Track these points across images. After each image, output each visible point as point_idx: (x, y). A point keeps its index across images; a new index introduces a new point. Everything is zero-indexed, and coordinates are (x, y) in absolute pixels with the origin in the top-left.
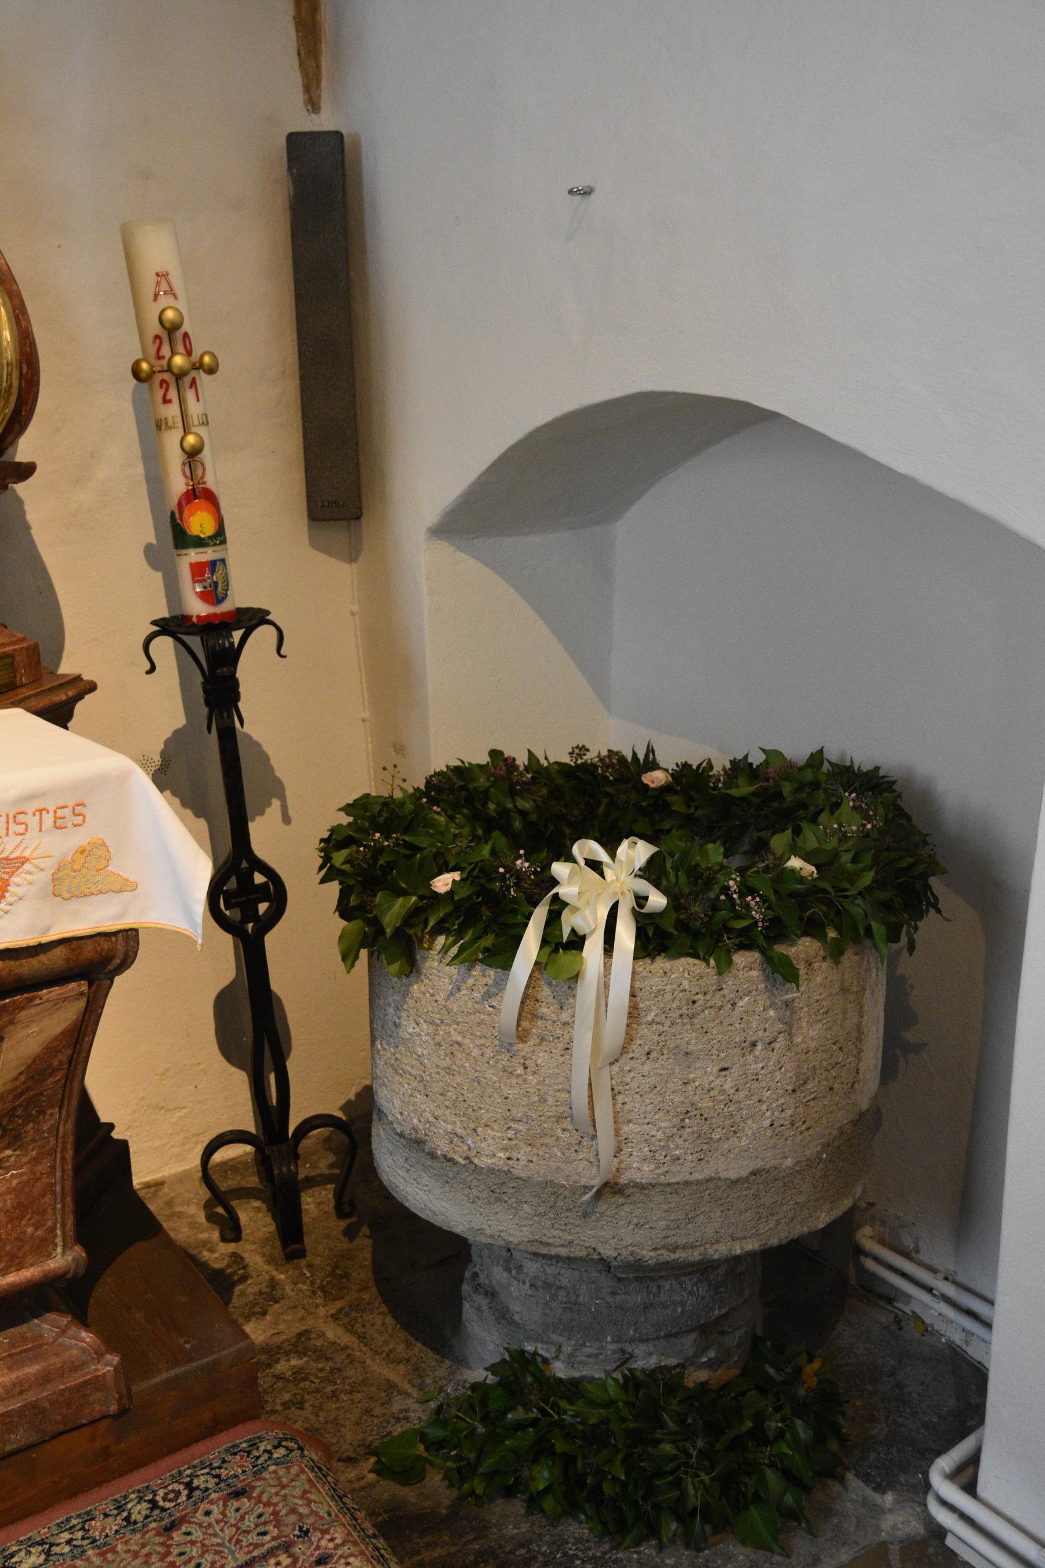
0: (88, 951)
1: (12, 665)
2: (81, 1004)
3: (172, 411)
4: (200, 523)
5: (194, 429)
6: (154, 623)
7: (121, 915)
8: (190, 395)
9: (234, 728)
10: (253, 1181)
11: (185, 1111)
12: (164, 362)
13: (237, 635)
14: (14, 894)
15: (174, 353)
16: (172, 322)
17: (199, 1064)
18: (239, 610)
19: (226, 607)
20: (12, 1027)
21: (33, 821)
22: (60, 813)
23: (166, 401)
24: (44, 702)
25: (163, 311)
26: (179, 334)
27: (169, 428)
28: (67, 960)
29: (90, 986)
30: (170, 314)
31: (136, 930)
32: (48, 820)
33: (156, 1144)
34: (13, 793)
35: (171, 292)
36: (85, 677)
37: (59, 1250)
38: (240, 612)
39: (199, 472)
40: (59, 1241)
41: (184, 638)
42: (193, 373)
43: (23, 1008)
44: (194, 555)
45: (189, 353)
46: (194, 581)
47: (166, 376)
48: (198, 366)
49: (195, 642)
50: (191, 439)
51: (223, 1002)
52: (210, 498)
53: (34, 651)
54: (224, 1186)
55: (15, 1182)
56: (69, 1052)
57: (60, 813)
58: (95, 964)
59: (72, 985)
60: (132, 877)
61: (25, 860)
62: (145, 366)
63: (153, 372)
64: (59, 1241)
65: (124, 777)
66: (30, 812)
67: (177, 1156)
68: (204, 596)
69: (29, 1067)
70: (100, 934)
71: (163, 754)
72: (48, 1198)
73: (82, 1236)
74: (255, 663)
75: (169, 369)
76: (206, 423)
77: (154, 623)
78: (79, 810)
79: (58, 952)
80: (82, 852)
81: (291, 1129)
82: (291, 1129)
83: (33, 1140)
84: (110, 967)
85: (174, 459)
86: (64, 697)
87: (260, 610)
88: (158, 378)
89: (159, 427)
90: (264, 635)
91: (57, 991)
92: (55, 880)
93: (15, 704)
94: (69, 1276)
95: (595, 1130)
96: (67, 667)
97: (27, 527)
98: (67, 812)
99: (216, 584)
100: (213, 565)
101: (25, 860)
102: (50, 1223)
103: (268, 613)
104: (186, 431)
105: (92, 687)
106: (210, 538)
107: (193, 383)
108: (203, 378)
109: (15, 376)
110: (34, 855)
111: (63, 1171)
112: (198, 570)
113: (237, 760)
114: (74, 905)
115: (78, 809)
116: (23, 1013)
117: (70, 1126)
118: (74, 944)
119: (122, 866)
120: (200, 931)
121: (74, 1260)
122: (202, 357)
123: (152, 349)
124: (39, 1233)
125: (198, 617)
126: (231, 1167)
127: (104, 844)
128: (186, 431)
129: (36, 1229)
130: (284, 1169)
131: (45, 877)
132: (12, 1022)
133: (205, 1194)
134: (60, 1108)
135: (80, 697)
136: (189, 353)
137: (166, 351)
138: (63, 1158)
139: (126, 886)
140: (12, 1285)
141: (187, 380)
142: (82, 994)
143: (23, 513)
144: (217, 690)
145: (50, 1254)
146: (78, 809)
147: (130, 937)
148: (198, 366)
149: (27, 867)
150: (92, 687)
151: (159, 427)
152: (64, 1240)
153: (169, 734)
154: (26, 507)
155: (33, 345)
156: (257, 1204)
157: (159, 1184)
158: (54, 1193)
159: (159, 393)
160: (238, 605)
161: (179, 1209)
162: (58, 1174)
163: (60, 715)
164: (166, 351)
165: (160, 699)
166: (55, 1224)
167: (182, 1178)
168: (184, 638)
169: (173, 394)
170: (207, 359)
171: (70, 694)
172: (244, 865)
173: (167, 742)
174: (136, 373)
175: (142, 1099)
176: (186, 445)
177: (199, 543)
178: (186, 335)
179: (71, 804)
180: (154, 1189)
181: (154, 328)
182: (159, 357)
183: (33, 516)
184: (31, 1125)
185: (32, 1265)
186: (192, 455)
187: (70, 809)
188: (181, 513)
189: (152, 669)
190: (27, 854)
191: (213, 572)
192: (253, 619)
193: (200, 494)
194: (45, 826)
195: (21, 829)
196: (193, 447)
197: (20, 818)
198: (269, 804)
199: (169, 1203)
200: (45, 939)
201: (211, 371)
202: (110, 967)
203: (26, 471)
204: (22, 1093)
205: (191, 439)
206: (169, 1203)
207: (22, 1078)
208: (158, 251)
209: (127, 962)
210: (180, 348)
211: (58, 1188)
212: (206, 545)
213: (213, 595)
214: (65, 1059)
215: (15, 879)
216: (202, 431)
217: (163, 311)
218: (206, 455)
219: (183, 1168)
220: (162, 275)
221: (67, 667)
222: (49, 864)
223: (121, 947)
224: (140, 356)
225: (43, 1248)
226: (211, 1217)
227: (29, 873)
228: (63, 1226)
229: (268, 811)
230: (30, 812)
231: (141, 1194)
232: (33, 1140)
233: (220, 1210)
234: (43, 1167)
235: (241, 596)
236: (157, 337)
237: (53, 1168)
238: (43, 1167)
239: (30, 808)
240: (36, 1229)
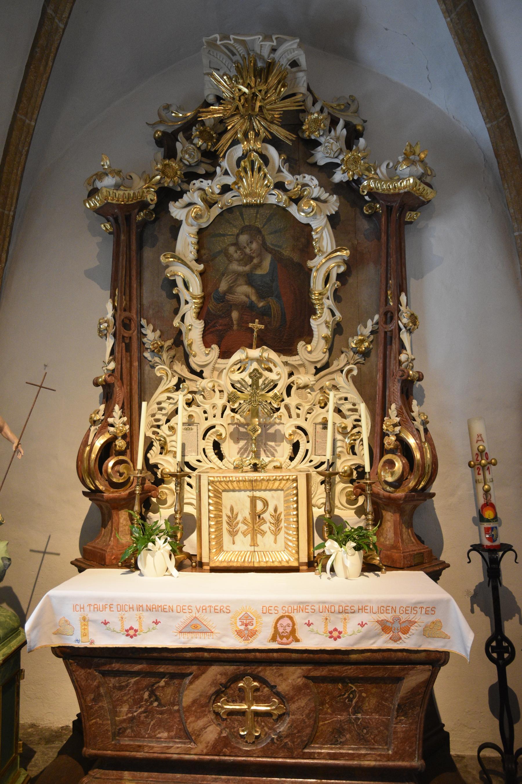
0: (433, 656)
1: (423, 556)
2: (429, 673)
3: (481, 477)
4: (489, 514)
5: (488, 484)
6: (471, 546)
7: (444, 646)
8: (487, 473)
9: (498, 587)
10: (500, 769)
11: (475, 730)
12: (479, 462)
13: (501, 553)
14: (411, 632)
15: (482, 459)
16: (482, 450)
17: (481, 712)
18: (502, 544)
19: (497, 543)
20: (407, 675)
21: (419, 610)
22: (427, 609)
23: (479, 474)
24: (431, 570)
25: (479, 446)
26: (484, 453)
27: (479, 483)
28: (426, 657)
29: (433, 668)
30: (481, 447)
31: (449, 653)
32: (424, 611)
33: (463, 740)
34: (414, 601)
35: (482, 440)
36: (446, 562)
37: (416, 759)
38: (502, 544)
39: (489, 498)
40: (416, 755)
41: (482, 552)
42: (488, 465)
43: (411, 670)
44: (486, 525)
45: (487, 459)
46: (486, 534)
47: (479, 466)
48: (490, 463)
49: (486, 555)
50: (486, 487)
51: (492, 689)
52: (493, 506)
53: (430, 552)
54: (487, 767)
55: (404, 729)
56: (425, 689)
57: (427, 609)
58: (436, 660)
59: (427, 666)
60: (449, 635)
61: (415, 622)
62: (472, 463)
63: (475, 465)
64: (416, 755)
65: (448, 601)
66: (418, 607)
67: (471, 748)
68: (490, 539)
69: (412, 690)
70: (437, 651)
71: (475, 590)
72: (414, 738)
73: (425, 756)
74: (507, 562)
75: (480, 464)
76: (492, 481)
77: (471, 546)
78: (433, 609)
79: (423, 654)
80: (433, 623)
81: (515, 751)
82: (515, 751)
83: (411, 716)
84: (440, 663)
85: (481, 493)
86: (438, 569)
87: (510, 545)
88: (477, 466)
89: (476, 482)
90: (509, 555)
91: (422, 667)
92: (424, 630)
93: (421, 570)
94: (419, 770)
95: (214, 570)
96: (442, 558)
97: (434, 509)
98: (429, 609)
99: (493, 535)
100: (492, 529)
101: (415, 622)
102: (414, 748)
103: (512, 546)
104: (485, 484)
105: (448, 566)
106: (492, 519)
107: (488, 468)
108: (492, 468)
109: (430, 468)
110: (419, 621)
111: (420, 730)
112: (487, 530)
113: (498, 597)
114: (430, 640)
115: (433, 609)
116: (411, 672)
117: (424, 714)
118: (428, 653)
119: (446, 630)
120: (469, 657)
121: (421, 765)
122: (491, 460)
123: (475, 458)
124: (410, 750)
125: (487, 546)
126: (490, 760)
127: (440, 622)
128: (485, 484)
129: (410, 748)
130: (510, 766)
131: (421, 629)
132: (407, 674)
133: (479, 768)
134: (421, 707)
135: (444, 569)
136: (487, 459)
137: (479, 458)
138: (420, 726)
139: (446, 637)
140: (400, 766)
141: (486, 468)
142: (430, 670)
143: (433, 504)
144: (493, 571)
145: (413, 760)
146: (433, 609)
147: (447, 654)
148: (490, 463)
149: (416, 624)
150: (448, 566)
151: (476, 482)
152: (418, 756)
153: (477, 584)
154: (434, 502)
155: (437, 459)
156: (501, 779)
157: (462, 757)
158: (416, 737)
159: (477, 471)
160: (501, 542)
161: (469, 770)
162: (418, 731)
163: (435, 576)
164: (479, 458)
165: (475, 572)
166: (416, 749)
167: (472, 758)
168: (482, 552)
169: (481, 472)
170: (493, 461)
171: (440, 567)
172: (499, 637)
173: (477, 586)
174: (470, 465)
175: (459, 720)
176: (484, 489)
177: (488, 521)
178: (486, 453)
179: (431, 607)
180: (460, 758)
181: (476, 451)
182: (477, 460)
183: (436, 506)
184: (410, 711)
185: (407, 761)
186: (487, 492)
187: (431, 608)
188: (482, 511)
189: (470, 562)
190: (416, 620)
191: (492, 531)
192: (507, 548)
193: (489, 505)
194: (422, 613)
195: (415, 612)
196: (487, 489)
197: (415, 609)
198: (514, 616)
199: (466, 766)
200: (420, 649)
201: (494, 465)
202: (440, 663)
203: (433, 495)
204: (409, 699)
205: (486, 487)
206: (466, 766)
207: (409, 693)
208: (478, 428)
209: (445, 662)
210: (485, 458)
211: (418, 736)
212: (490, 522)
213: (492, 539)
214: (423, 691)
215: (412, 628)
216: (491, 484)
217: (479, 446)
218: (492, 492)
219: (471, 754)
220: (479, 436)
221: (442, 558)
222: (423, 625)
223: (443, 657)
224: (471, 460)
225: (411, 757)
226: (481, 778)
227: (416, 626)
228: (418, 751)
229: (514, 618)
230: (418, 607)
231: (454, 759)
232: (411, 716)
233: (485, 776)
234: (413, 727)
235: (503, 539)
236: (477, 454)
237: (417, 728)
238: (413, 727)
239: (418, 606)
240: (410, 748)
